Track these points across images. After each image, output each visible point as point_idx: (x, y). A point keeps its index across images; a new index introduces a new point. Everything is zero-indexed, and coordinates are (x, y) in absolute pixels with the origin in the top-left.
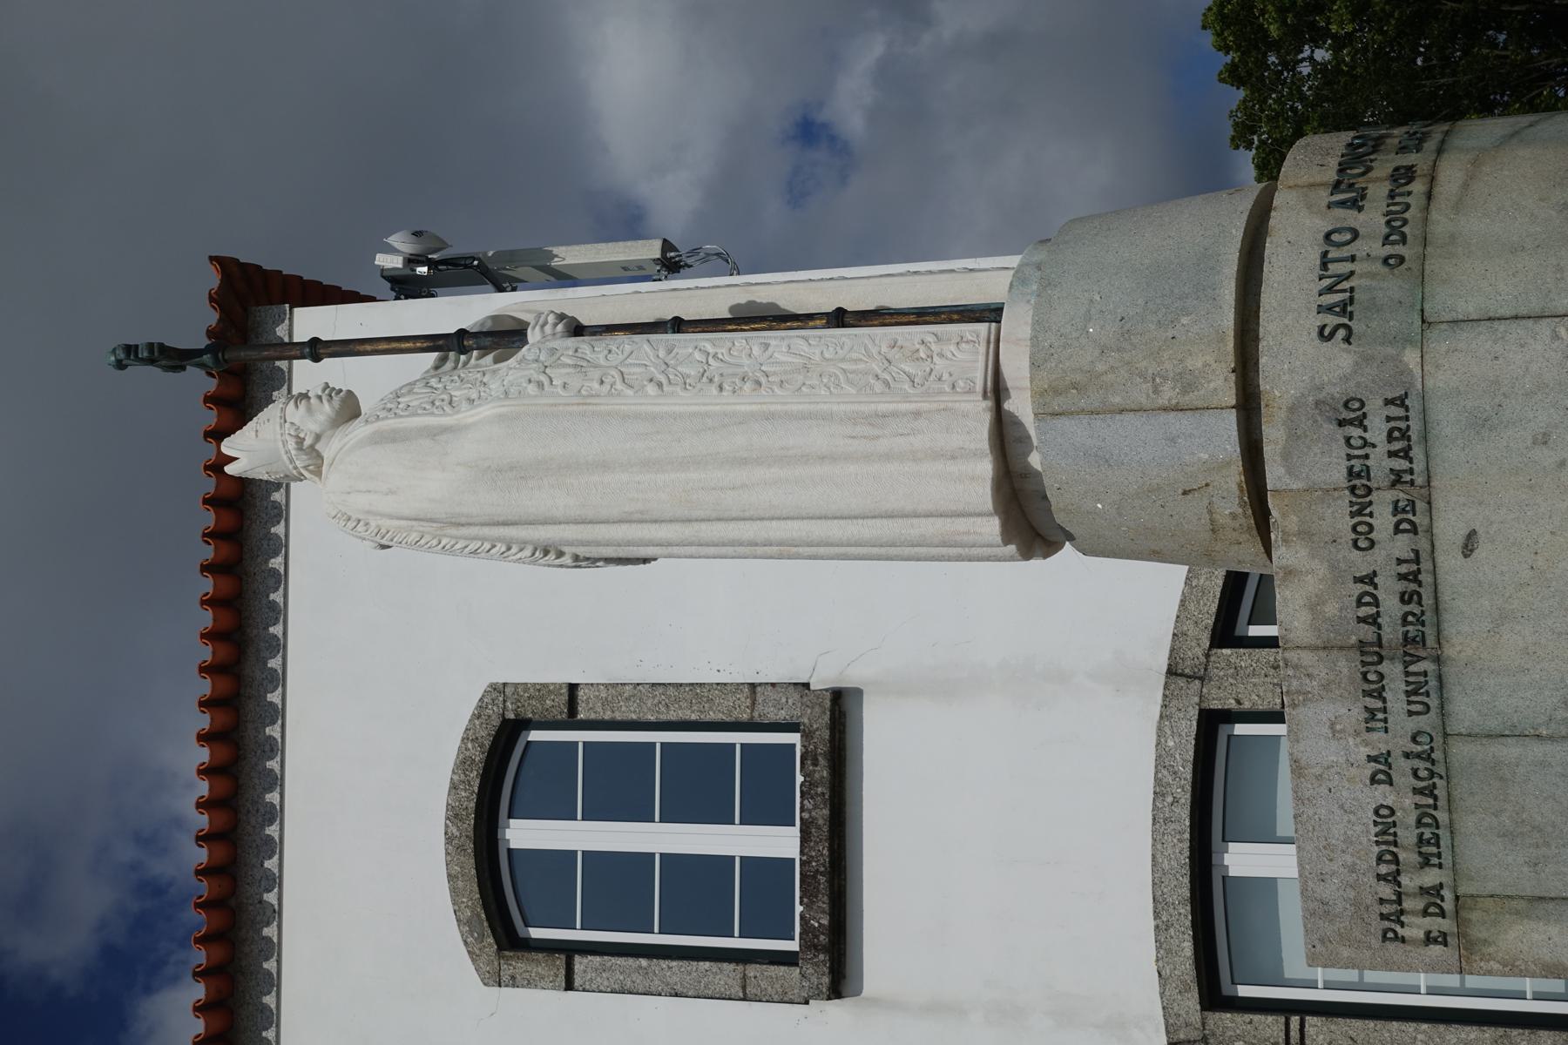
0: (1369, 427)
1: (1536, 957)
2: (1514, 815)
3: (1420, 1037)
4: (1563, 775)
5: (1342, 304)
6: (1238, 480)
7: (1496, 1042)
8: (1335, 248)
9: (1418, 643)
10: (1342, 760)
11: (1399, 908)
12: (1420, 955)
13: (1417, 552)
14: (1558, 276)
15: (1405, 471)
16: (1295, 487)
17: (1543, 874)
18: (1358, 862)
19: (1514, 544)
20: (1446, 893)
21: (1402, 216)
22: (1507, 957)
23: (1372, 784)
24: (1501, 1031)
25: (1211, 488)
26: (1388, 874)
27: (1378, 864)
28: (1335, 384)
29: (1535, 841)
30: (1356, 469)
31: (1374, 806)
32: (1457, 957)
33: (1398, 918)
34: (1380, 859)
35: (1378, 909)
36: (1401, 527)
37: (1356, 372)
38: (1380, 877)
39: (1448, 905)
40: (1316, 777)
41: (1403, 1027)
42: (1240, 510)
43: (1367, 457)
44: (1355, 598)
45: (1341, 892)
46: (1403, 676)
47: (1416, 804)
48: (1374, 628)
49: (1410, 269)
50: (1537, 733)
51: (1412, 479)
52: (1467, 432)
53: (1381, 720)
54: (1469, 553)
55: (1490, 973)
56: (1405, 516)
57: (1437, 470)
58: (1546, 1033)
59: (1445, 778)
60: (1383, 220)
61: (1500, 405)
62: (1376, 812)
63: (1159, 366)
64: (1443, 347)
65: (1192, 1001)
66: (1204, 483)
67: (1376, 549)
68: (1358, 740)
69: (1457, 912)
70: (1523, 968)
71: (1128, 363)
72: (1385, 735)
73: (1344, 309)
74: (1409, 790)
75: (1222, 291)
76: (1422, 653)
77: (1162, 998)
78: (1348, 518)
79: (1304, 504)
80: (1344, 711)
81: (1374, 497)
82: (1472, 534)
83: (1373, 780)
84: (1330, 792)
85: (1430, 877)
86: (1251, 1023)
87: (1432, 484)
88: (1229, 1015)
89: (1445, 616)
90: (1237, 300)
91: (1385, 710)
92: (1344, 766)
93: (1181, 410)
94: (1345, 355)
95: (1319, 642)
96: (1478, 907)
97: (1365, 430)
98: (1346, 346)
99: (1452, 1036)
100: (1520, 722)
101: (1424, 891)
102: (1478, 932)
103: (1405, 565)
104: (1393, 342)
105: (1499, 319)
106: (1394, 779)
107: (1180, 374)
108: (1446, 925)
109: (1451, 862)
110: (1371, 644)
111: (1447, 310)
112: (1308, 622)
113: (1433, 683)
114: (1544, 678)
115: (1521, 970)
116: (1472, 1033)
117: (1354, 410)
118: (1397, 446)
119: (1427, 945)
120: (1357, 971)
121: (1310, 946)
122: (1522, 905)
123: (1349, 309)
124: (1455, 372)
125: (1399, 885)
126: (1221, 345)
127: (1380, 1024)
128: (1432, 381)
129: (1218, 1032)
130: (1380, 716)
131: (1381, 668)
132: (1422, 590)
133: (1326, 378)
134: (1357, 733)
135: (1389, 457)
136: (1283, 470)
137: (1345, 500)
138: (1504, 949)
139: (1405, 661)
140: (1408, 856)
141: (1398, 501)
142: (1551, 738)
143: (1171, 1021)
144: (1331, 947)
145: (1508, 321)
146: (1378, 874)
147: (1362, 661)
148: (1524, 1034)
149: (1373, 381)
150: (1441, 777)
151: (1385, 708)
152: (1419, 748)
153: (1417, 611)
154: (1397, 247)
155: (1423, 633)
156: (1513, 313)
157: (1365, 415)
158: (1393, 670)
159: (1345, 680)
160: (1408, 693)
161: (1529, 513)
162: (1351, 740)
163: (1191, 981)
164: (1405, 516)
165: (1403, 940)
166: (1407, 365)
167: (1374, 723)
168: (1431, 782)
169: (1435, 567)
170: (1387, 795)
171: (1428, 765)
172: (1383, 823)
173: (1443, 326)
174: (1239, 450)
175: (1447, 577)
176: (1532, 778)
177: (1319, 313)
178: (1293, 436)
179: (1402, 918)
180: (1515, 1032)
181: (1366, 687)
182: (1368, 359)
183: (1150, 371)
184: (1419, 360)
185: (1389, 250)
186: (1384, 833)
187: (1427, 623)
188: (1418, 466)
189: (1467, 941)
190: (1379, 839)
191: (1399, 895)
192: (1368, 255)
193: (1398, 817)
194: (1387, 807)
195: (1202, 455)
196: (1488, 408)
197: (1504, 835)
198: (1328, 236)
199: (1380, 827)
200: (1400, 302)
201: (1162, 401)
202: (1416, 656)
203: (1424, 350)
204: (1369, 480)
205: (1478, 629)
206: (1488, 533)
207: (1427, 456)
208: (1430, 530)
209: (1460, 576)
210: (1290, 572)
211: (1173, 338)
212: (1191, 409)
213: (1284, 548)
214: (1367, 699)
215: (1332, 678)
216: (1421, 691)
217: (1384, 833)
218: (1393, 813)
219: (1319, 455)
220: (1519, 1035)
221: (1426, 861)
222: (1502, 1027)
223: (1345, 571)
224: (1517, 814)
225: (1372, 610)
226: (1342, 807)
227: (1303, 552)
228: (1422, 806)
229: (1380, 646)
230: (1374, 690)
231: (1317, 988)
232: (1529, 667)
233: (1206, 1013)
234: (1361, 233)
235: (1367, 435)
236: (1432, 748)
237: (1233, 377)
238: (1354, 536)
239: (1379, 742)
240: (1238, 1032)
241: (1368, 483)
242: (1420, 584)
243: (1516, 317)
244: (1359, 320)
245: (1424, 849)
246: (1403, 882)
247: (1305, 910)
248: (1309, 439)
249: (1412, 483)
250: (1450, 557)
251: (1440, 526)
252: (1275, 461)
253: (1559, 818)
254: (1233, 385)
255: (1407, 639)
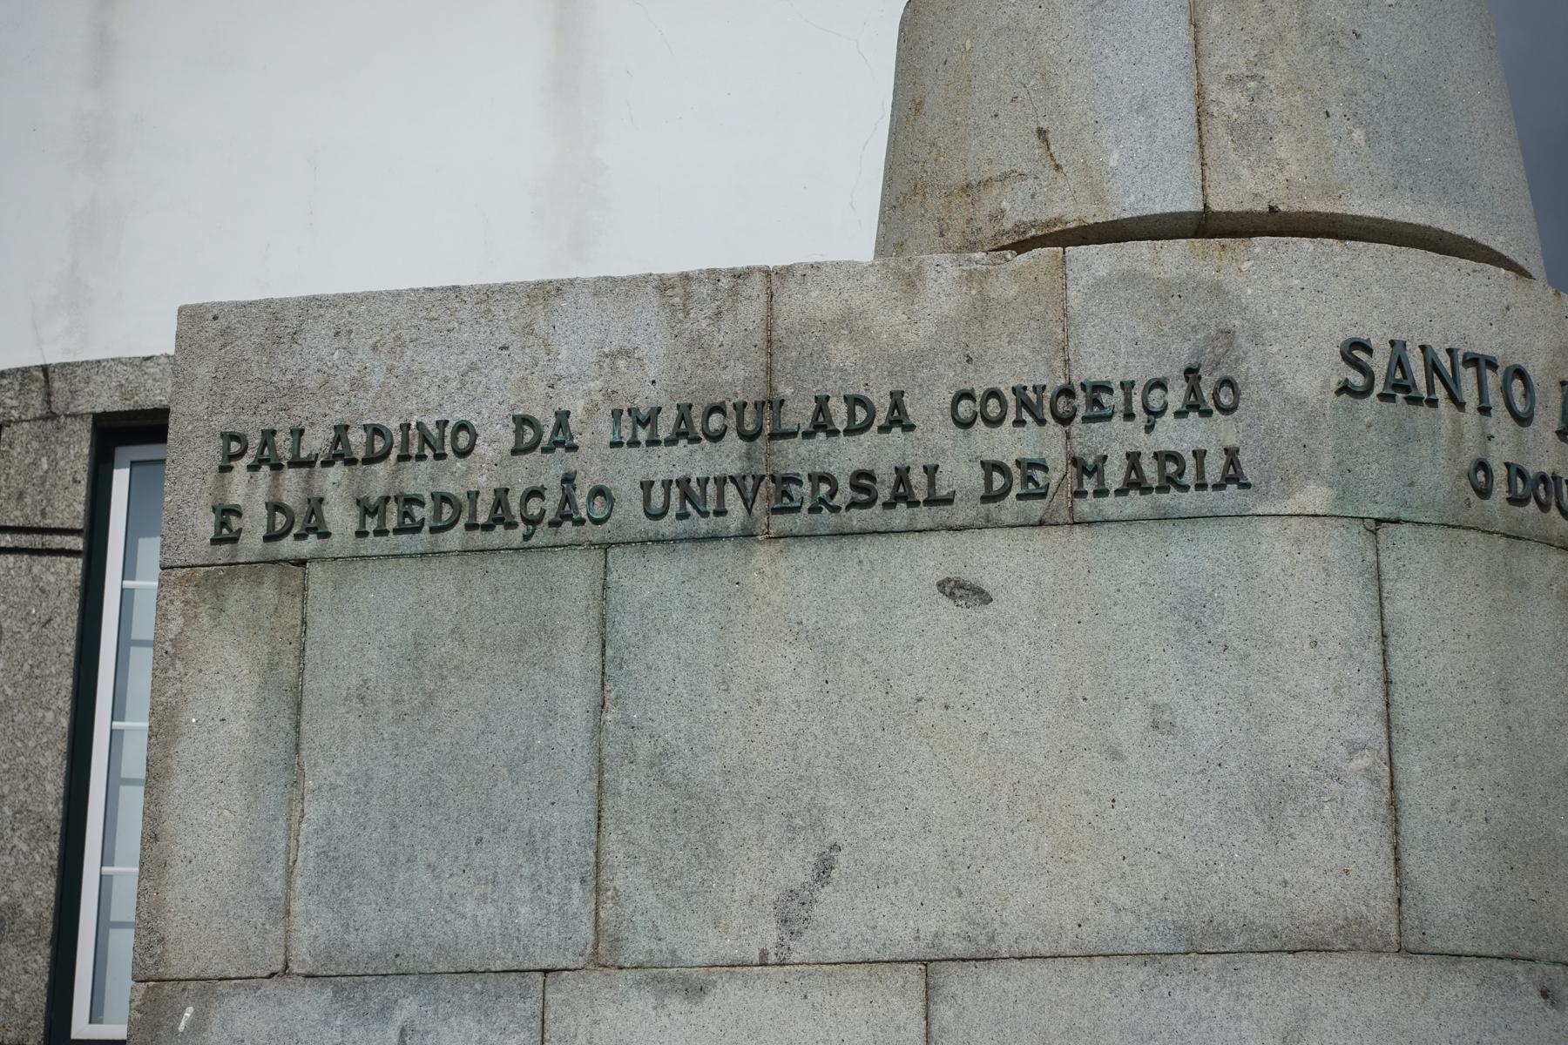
0: (1184, 421)
1: (190, 697)
2: (455, 662)
3: (50, 716)
4: (528, 749)
5: (1406, 383)
6: (1069, 217)
7: (40, 820)
8: (1500, 383)
9: (779, 500)
10: (560, 369)
11: (285, 463)
12: (197, 498)
13: (948, 501)
14: (1461, 759)
15: (1101, 481)
16: (1072, 293)
17: (344, 710)
18: (369, 396)
19: (964, 668)
20: (311, 544)
21: (1554, 503)
22: (190, 647)
23: (514, 418)
24: (56, 827)
25: (1052, 173)
26: (347, 445)
27: (365, 427)
28: (1264, 364)
29: (406, 698)
30: (1104, 398)
31: (474, 423)
32: (192, 561)
33: (266, 461)
34: (377, 431)
35: (283, 426)
36: (995, 474)
37: (1286, 400)
38: (342, 430)
39: (288, 547)
40: (530, 325)
41: (63, 693)
42: (1008, 226)
43: (1129, 416)
44: (863, 393)
45: (316, 365)
46: (717, 474)
47: (477, 493)
48: (806, 425)
49: (1469, 505)
50: (607, 704)
51: (1086, 493)
52: (1175, 590)
53: (634, 435)
54: (948, 590)
55: (162, 616)
56: (1017, 481)
57: (1105, 538)
58: (53, 890)
59: (526, 545)
60: (1546, 469)
61: (1226, 648)
62: (463, 426)
63: (1277, 87)
64: (1333, 553)
65: (108, 401)
66: (1062, 162)
67: (954, 431)
68: (598, 397)
69: (274, 562)
70: (171, 673)
71: (1281, 38)
72: (606, 442)
73: (1400, 387)
74: (504, 483)
75: (1409, 201)
76: (759, 507)
77: (113, 360)
78: (1014, 383)
79: (1039, 308)
80: (652, 373)
81: (1053, 427)
82: (981, 596)
83: (523, 421)
84: (501, 348)
85: (340, 517)
86: (75, 481)
87: (1077, 529)
88: (86, 451)
89: (828, 549)
90: (1394, 223)
91: (653, 442)
92: (550, 373)
93: (1199, 121)
94: (1317, 383)
95: (780, 332)
96: (284, 598)
97: (1179, 414)
98: (1334, 386)
99: (50, 760)
100: (629, 674)
101: (315, 505)
102: (238, 597)
103: (924, 480)
104: (1342, 467)
105: (1384, 652)
106: (525, 457)
107: (1265, 121)
108: (252, 543)
109: (369, 552)
110: (776, 420)
111: (1400, 564)
112: (818, 314)
113: (703, 526)
114: (712, 717)
115: (165, 670)
116: (54, 785)
117: (1215, 396)
118: (1150, 470)
119: (214, 509)
120: (151, 637)
121: (216, 311)
122: (288, 674)
123: (1400, 396)
124: (1290, 571)
125: (326, 464)
126: (1319, 192)
127: (69, 660)
128: (1269, 531)
129: (61, 435)
130: (642, 435)
131: (732, 437)
132: (877, 508)
133: (1275, 349)
134: (610, 395)
135: (1128, 455)
136: (1103, 273)
137: (1044, 375)
138: (206, 641)
139: (744, 477)
140: (379, 480)
141: (1045, 469)
142: (599, 727)
143: (79, 371)
144: (215, 346)
145: (1381, 667)
146: (347, 427)
147: (745, 404)
148: (51, 858)
149: (1270, 431)
150: (526, 537)
151: (657, 443)
152: (581, 500)
153: (839, 500)
154: (1504, 487)
155: (797, 510)
156: (1395, 677)
157: (1206, 413)
158: (729, 456)
159: (710, 375)
160: (684, 483)
161: (1022, 695)
162: (597, 384)
163: (137, 402)
164: (1017, 481)
165: (225, 469)
166: (1301, 489)
167: (629, 424)
168: (518, 519)
169: (919, 531)
170: (495, 446)
171: (549, 516)
172: (443, 437)
173: (1370, 556)
174: (1126, 215)
175: (902, 552)
176: (523, 694)
177: (1392, 343)
178: (1167, 292)
179: (265, 468)
180: (54, 846)
181: (697, 412)
182: (1311, 421)
183: (1267, 73)
184: (1310, 510)
185: (1500, 473)
186: (425, 439)
187: (815, 516)
188: (1110, 506)
189: (220, 578)
190: (413, 431)
191: (309, 463)
192: (1490, 438)
193: (455, 463)
194: (472, 445)
195: (1116, 156)
196: (1221, 627)
197: (417, 645)
198: (1520, 373)
199: (435, 432)
200: (1412, 484)
201: (1214, 90)
202: (755, 497)
203: (1327, 520)
204: (1085, 419)
205: (805, 603)
206: (985, 624)
207: (1130, 521)
208: (990, 524)
209: (904, 575)
210: (912, 284)
211: (1327, 114)
212: (1200, 137)
213: (956, 274)
214: (674, 413)
215: (714, 353)
216: (689, 506)
217: (425, 439)
218: (463, 454)
219: (1130, 335)
220: (51, 852)
221: (372, 510)
222: (62, 829)
223: (914, 378)
224: (456, 668)
225: (840, 421)
226: (473, 367)
227: (948, 306)
228: (473, 503)
229: (773, 436)
230: (690, 424)
231: (112, 720)
232: (732, 693)
233: (90, 420)
234: (1525, 429)
235: (1169, 417)
236: (581, 522)
237: (1262, 207)
238: (979, 393)
239: (593, 433)
240: (62, 463)
241: (1078, 419)
242: (888, 505)
243: (1388, 682)
244: (1380, 412)
245: (393, 507)
246: (331, 470)
247: (284, 303)
248: (1162, 318)
249: (1080, 494)
250: (941, 559)
251: (996, 541)
252: (1120, 259)
253: (448, 741)
254: (1247, 207)
255: (785, 481)
